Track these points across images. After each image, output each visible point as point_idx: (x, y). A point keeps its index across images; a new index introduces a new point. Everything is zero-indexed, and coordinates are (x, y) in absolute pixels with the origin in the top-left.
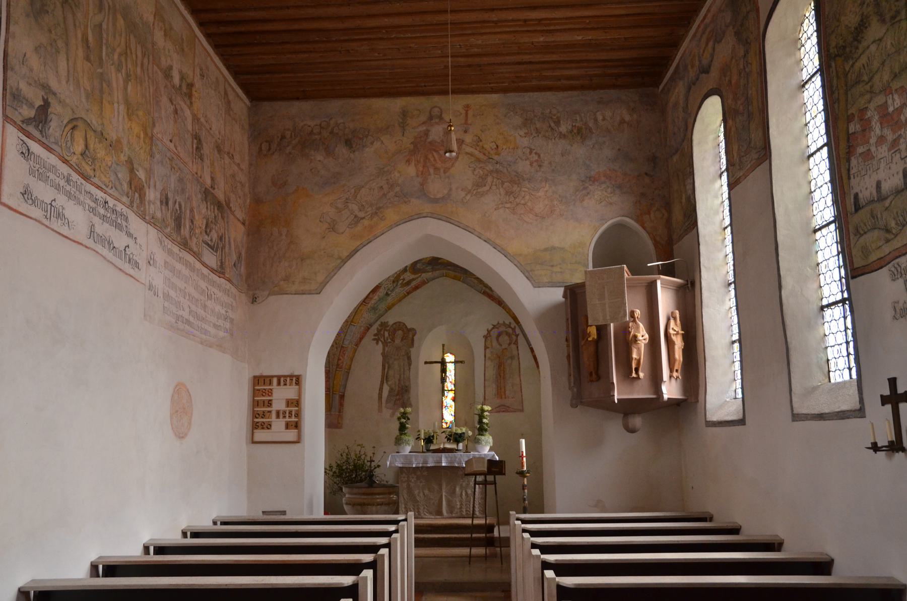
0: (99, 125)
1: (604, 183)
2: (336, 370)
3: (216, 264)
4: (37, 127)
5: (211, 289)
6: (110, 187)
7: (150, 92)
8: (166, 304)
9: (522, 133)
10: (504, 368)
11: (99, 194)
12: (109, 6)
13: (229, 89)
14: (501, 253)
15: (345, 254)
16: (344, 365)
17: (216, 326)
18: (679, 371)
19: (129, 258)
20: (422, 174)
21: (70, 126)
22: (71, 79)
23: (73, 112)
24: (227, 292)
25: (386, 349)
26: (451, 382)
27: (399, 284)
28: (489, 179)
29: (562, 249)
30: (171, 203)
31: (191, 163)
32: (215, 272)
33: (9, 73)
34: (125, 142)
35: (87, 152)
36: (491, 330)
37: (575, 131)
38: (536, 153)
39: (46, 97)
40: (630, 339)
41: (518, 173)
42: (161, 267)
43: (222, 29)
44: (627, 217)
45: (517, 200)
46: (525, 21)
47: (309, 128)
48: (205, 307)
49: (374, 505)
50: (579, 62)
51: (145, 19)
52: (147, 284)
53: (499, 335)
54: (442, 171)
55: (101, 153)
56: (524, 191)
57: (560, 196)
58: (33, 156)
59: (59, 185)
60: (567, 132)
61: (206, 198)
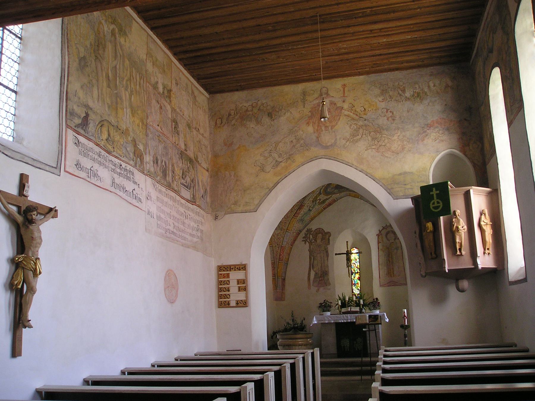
0: (115, 122)
2: (279, 262)
3: (190, 197)
4: (82, 128)
5: (187, 212)
6: (123, 156)
7: (144, 99)
8: (159, 222)
9: (380, 99)
10: (391, 256)
11: (117, 161)
12: (120, 55)
13: (194, 89)
15: (271, 185)
16: (284, 259)
17: (191, 235)
18: (490, 249)
19: (135, 196)
20: (317, 131)
21: (100, 125)
22: (100, 100)
23: (101, 117)
24: (198, 214)
26: (357, 267)
27: (317, 203)
28: (361, 131)
29: (412, 173)
30: (159, 162)
31: (171, 137)
32: (189, 201)
33: (69, 102)
34: (130, 129)
35: (109, 138)
36: (381, 231)
37: (416, 95)
38: (390, 112)
39: (87, 112)
40: (454, 230)
41: (379, 126)
42: (154, 201)
43: (188, 55)
44: (454, 149)
45: (379, 143)
46: (371, 31)
47: (245, 108)
48: (184, 223)
49: (296, 346)
50: (412, 51)
51: (141, 57)
52: (147, 211)
53: (387, 234)
54: (330, 128)
55: (117, 138)
56: (384, 137)
57: (408, 138)
58: (81, 144)
59: (95, 158)
61: (182, 157)
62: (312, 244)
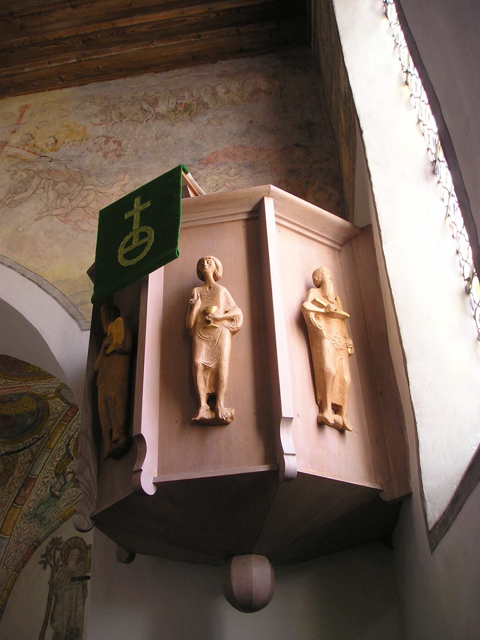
1: (224, 163)
14: (33, 282)
18: (345, 410)
25: (56, 575)
37: (181, 109)
40: (193, 323)
60: (168, 111)
62: (57, 570)
